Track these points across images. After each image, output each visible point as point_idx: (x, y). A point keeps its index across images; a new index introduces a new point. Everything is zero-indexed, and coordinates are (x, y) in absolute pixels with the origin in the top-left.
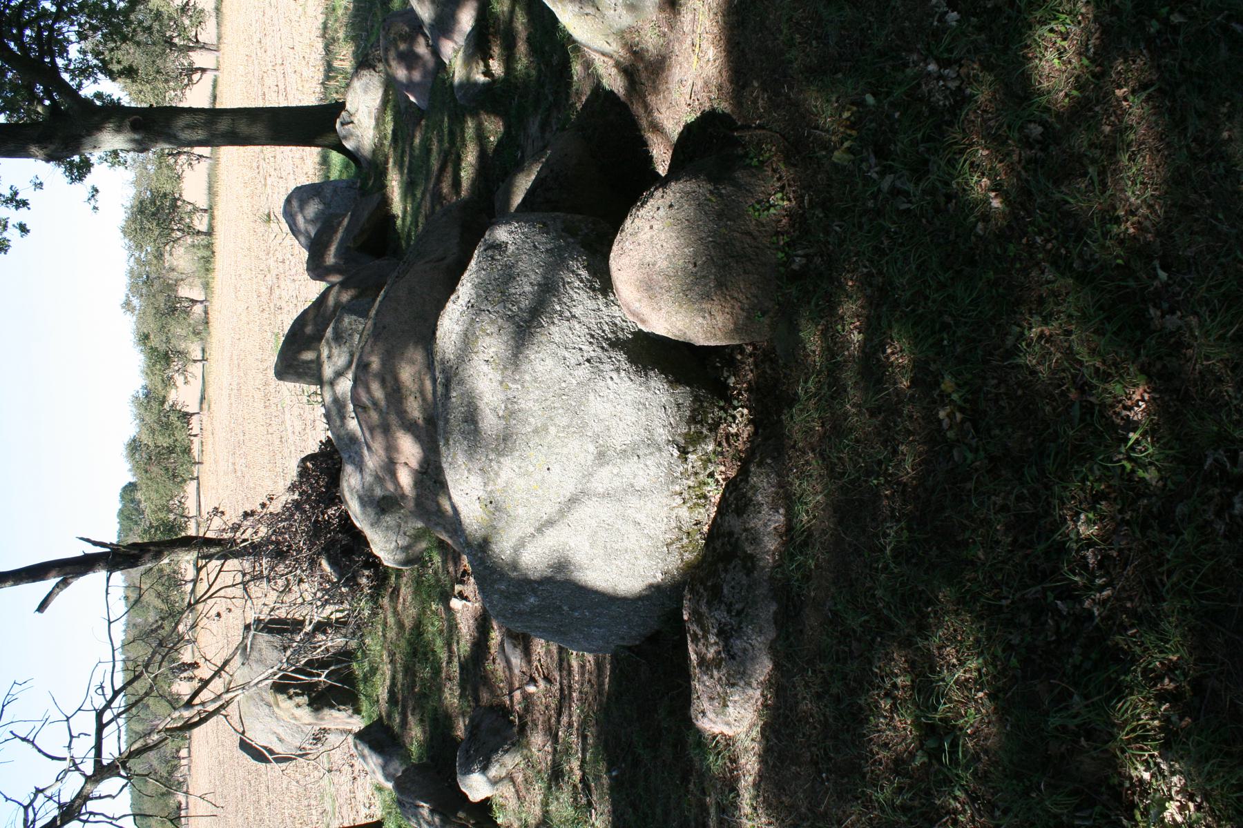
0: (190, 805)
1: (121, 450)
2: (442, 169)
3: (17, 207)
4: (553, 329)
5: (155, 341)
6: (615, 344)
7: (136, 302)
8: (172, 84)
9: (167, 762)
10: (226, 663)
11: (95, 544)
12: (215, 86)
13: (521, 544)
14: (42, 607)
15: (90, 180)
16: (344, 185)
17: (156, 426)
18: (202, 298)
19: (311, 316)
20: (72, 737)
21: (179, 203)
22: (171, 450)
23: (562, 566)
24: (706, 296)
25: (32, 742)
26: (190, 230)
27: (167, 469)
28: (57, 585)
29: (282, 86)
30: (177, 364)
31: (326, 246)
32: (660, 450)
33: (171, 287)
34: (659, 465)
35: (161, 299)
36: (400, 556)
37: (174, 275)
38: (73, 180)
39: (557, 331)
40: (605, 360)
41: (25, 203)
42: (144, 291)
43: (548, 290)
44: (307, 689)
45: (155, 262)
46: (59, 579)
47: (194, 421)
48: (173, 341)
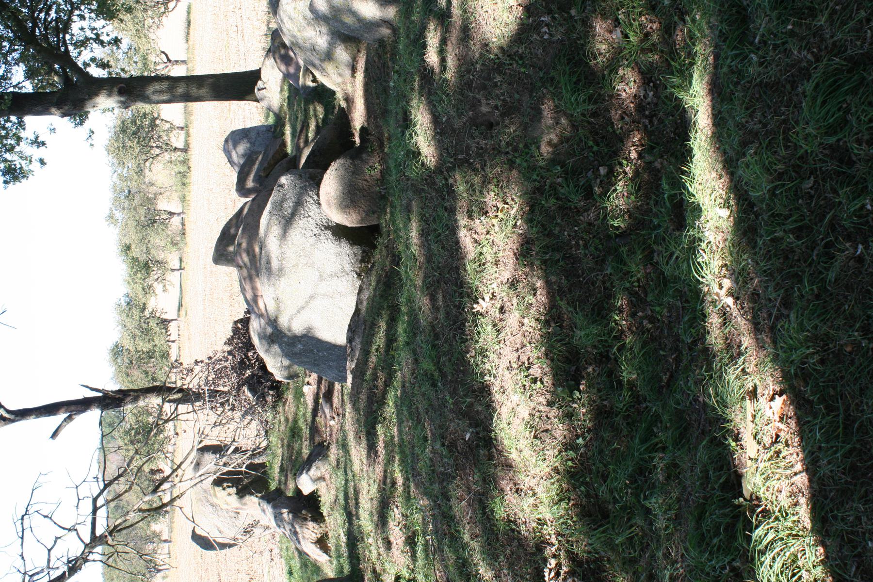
2: (301, 131)
5: (136, 252)
6: (327, 228)
7: (118, 215)
8: (150, 13)
10: (182, 463)
11: (92, 389)
14: (55, 435)
15: (88, 124)
16: (265, 129)
17: (138, 333)
19: (234, 221)
21: (158, 122)
22: (150, 355)
23: (309, 329)
24: (347, 207)
27: (147, 373)
28: (65, 420)
29: (240, 28)
30: (154, 275)
31: (248, 174)
35: (142, 211)
36: (285, 373)
37: (153, 189)
41: (43, 144)
42: (126, 205)
43: (299, 203)
44: (235, 483)
45: (136, 177)
46: (67, 415)
47: (172, 326)
48: (153, 251)
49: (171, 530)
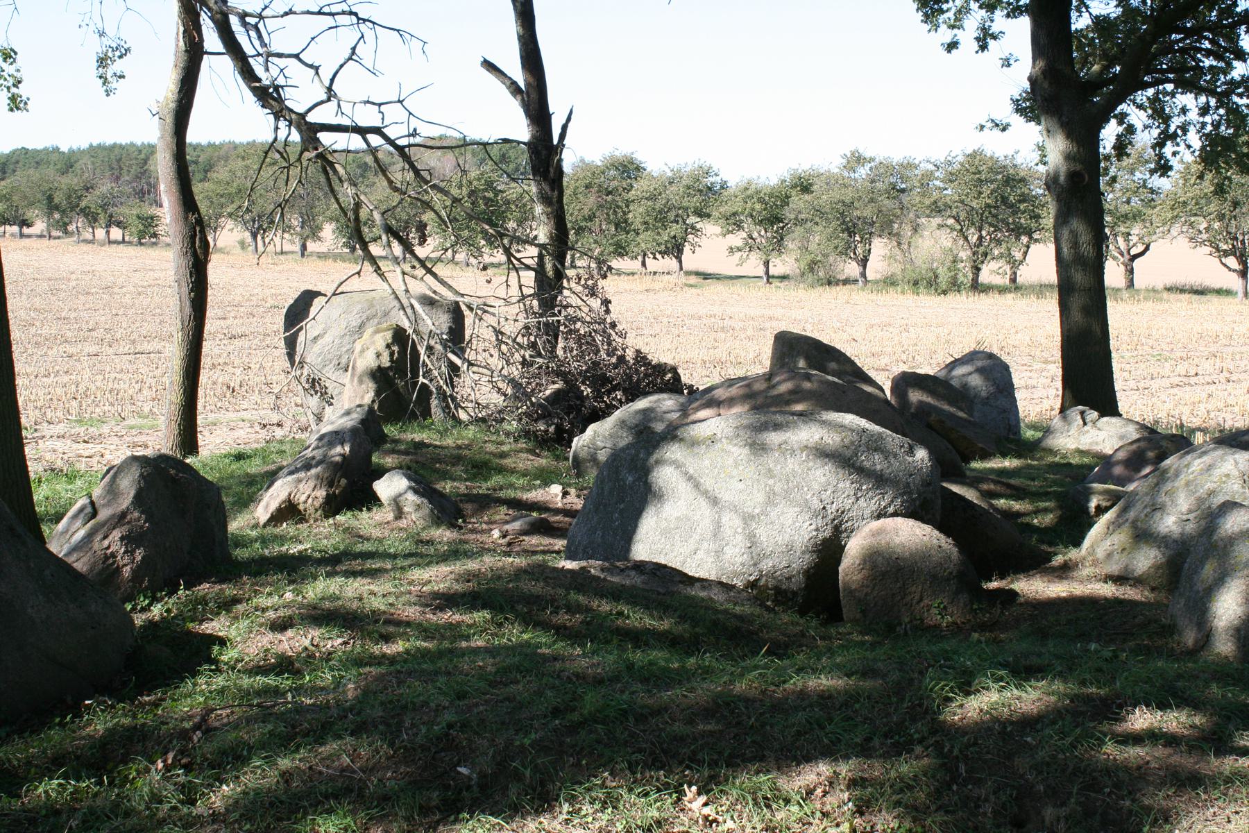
0: (26, 241)
1: (623, 148)
2: (1009, 486)
3: (978, 39)
4: (848, 483)
5: (798, 201)
6: (837, 530)
7: (863, 171)
8: (1216, 225)
9: (104, 207)
12: (1219, 292)
13: (677, 464)
14: (489, 66)
15: (1018, 121)
18: (870, 275)
20: (380, 105)
21: (1024, 239)
22: (622, 225)
24: (874, 567)
25: (350, 59)
26: (979, 257)
28: (514, 83)
30: (759, 233)
31: (932, 393)
32: (755, 565)
33: (886, 225)
34: (743, 564)
35: (868, 212)
37: (907, 231)
38: (1016, 102)
39: (846, 485)
40: (825, 521)
41: (984, 47)
42: (879, 185)
43: (880, 480)
45: (927, 202)
47: (670, 263)
48: (799, 231)
49: (322, 256)
